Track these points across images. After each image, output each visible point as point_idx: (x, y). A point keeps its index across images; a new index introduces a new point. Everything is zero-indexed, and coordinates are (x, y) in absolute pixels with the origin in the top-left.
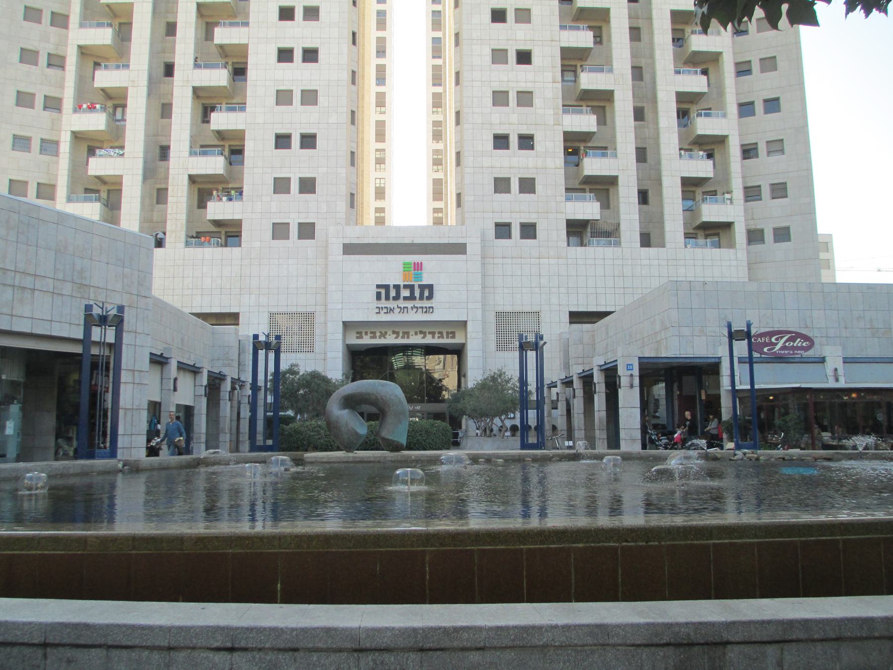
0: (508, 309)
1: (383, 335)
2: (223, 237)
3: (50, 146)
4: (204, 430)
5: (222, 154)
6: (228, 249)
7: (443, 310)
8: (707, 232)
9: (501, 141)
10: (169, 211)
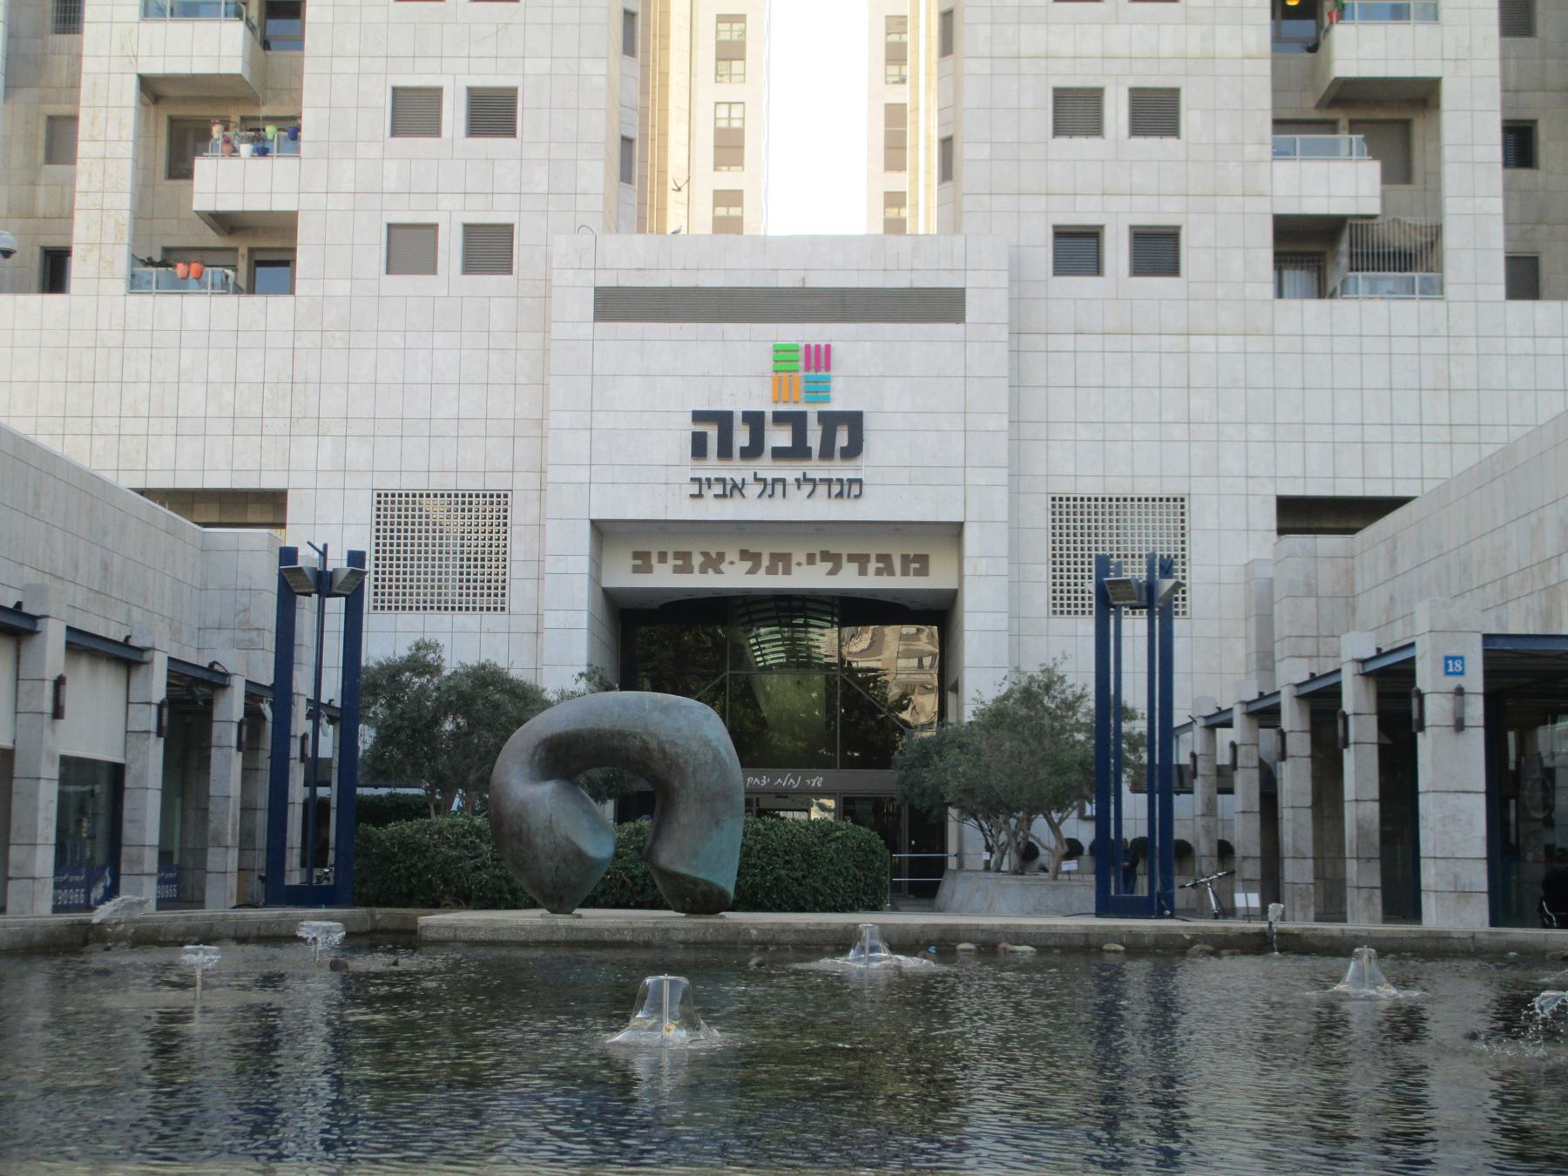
1: (713, 563)
2: (243, 266)
4: (152, 835)
5: (239, 15)
6: (256, 300)
7: (890, 489)
10: (81, 183)
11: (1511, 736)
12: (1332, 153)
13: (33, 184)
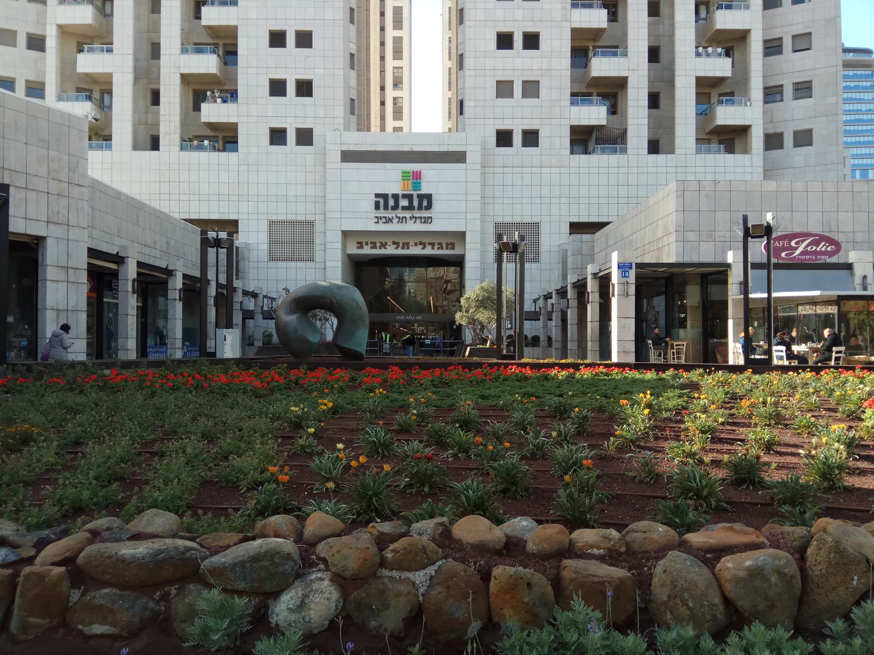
0: (508, 220)
1: (383, 245)
2: (221, 142)
3: (36, 43)
5: (215, 52)
7: (442, 220)
8: (722, 137)
9: (504, 41)
11: (645, 301)
12: (591, 103)
13: (147, 113)
